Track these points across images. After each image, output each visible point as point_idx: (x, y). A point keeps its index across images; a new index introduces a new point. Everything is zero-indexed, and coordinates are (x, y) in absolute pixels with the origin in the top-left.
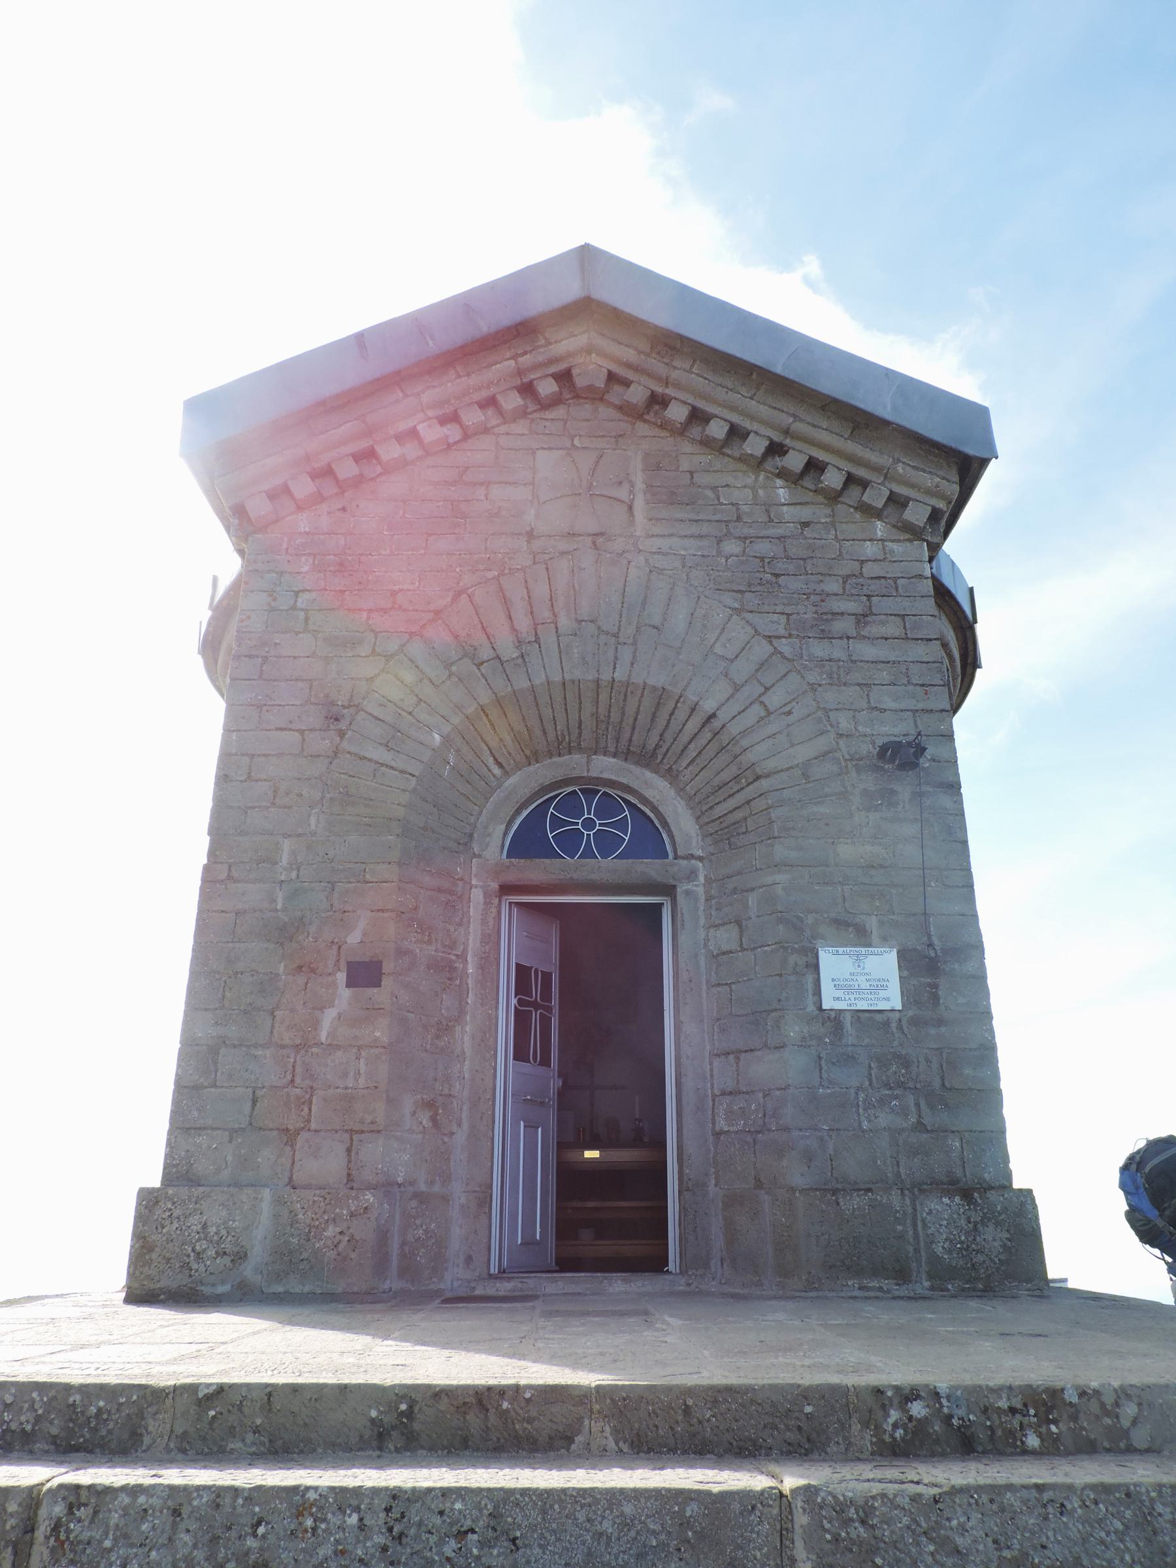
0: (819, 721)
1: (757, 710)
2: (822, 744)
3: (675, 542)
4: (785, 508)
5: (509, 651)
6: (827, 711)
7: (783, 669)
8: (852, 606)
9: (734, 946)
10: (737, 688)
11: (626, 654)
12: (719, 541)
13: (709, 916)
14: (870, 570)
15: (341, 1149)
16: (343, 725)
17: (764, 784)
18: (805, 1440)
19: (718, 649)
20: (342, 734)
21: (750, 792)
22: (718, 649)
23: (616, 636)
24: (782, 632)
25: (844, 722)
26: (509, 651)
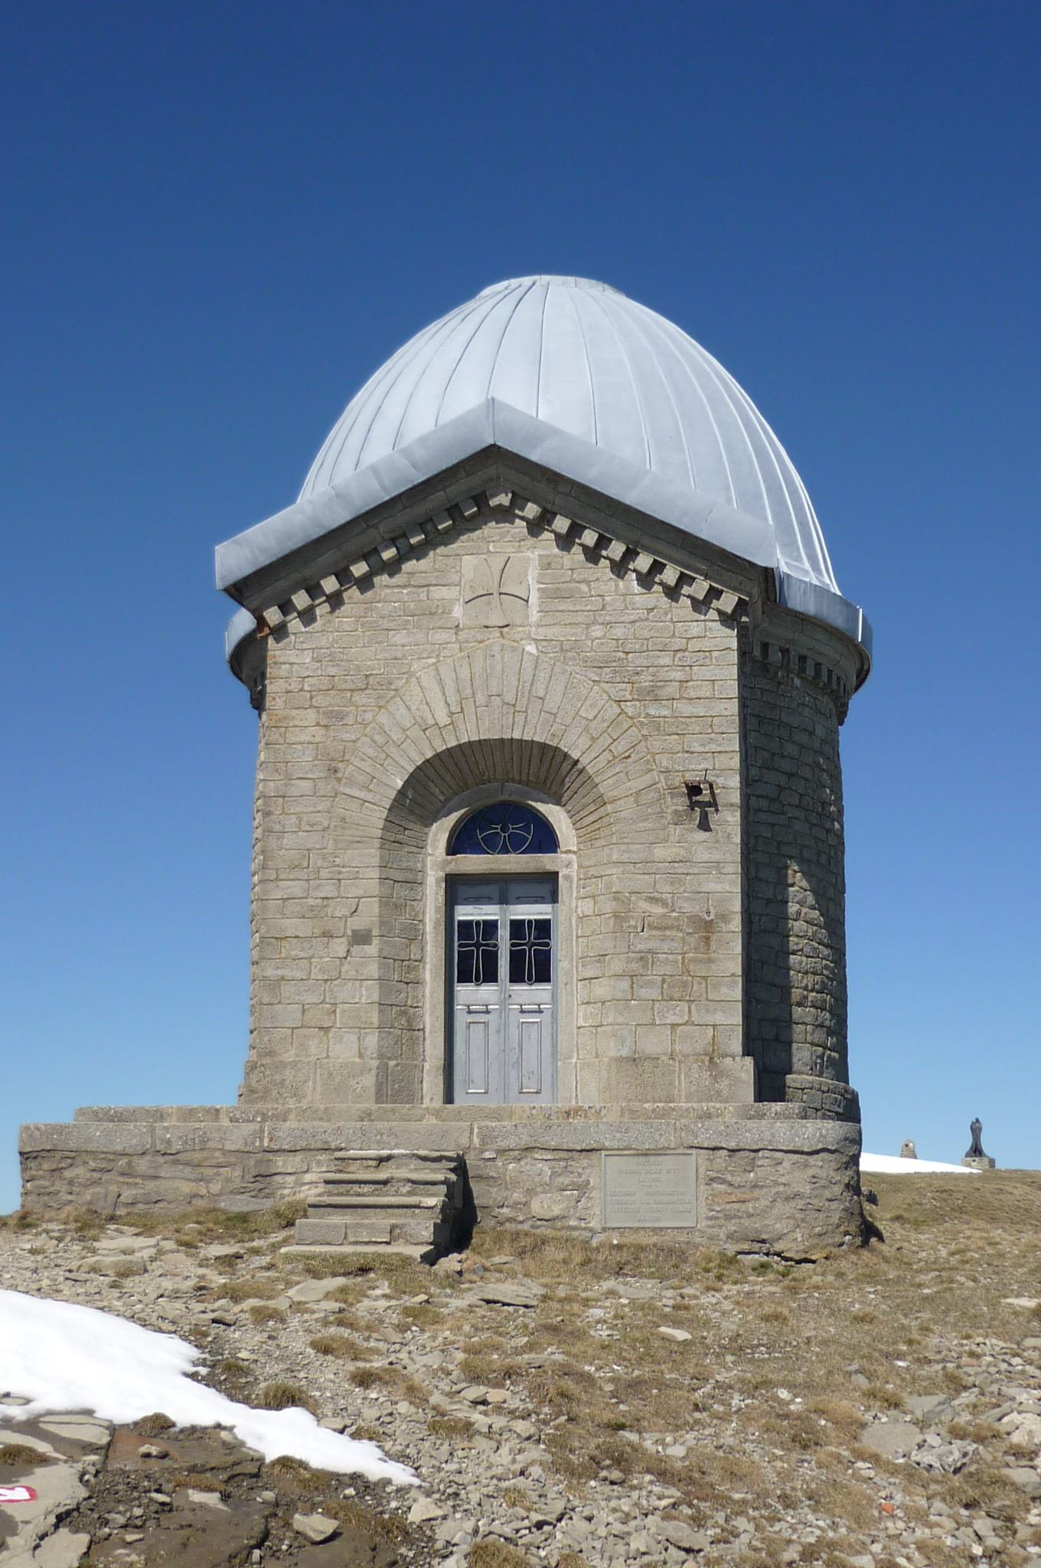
0: (648, 762)
1: (607, 755)
2: (647, 779)
3: (556, 630)
4: (637, 598)
5: (443, 719)
6: (653, 754)
7: (626, 725)
8: (678, 675)
9: (590, 913)
10: (594, 739)
11: (520, 718)
12: (588, 626)
13: (578, 892)
14: (694, 645)
15: (354, 1038)
16: (339, 775)
17: (609, 808)
18: (488, 1264)
19: (582, 713)
20: (339, 780)
21: (601, 812)
22: (582, 713)
23: (514, 705)
24: (629, 697)
25: (664, 761)
26: (443, 719)
